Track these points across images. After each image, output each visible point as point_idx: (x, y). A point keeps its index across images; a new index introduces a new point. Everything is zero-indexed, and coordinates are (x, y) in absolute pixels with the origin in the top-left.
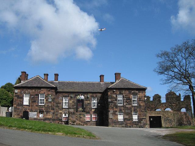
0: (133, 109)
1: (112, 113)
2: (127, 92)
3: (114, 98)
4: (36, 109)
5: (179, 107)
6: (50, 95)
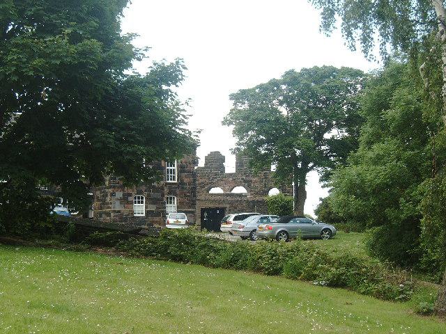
0: (166, 190)
1: (121, 199)
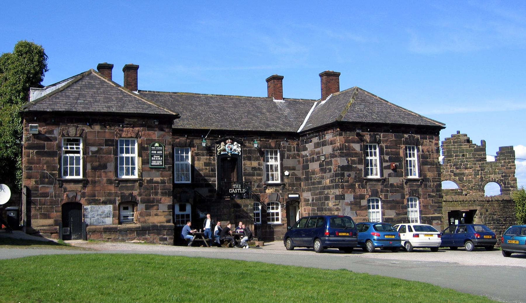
0: (407, 189)
1: (351, 204)
2: (392, 137)
3: (356, 154)
4: (110, 194)
5: (482, 178)
6: (157, 145)
